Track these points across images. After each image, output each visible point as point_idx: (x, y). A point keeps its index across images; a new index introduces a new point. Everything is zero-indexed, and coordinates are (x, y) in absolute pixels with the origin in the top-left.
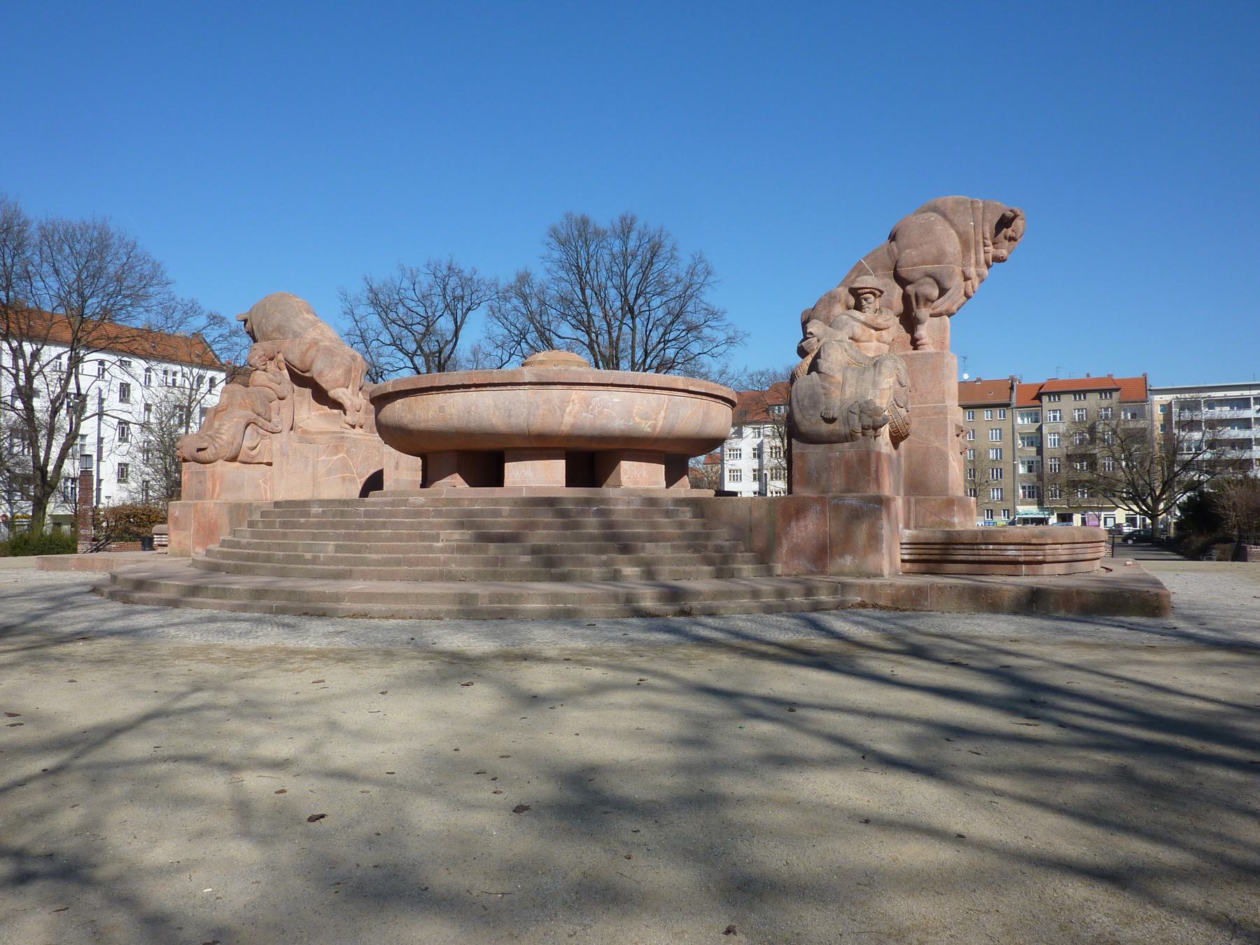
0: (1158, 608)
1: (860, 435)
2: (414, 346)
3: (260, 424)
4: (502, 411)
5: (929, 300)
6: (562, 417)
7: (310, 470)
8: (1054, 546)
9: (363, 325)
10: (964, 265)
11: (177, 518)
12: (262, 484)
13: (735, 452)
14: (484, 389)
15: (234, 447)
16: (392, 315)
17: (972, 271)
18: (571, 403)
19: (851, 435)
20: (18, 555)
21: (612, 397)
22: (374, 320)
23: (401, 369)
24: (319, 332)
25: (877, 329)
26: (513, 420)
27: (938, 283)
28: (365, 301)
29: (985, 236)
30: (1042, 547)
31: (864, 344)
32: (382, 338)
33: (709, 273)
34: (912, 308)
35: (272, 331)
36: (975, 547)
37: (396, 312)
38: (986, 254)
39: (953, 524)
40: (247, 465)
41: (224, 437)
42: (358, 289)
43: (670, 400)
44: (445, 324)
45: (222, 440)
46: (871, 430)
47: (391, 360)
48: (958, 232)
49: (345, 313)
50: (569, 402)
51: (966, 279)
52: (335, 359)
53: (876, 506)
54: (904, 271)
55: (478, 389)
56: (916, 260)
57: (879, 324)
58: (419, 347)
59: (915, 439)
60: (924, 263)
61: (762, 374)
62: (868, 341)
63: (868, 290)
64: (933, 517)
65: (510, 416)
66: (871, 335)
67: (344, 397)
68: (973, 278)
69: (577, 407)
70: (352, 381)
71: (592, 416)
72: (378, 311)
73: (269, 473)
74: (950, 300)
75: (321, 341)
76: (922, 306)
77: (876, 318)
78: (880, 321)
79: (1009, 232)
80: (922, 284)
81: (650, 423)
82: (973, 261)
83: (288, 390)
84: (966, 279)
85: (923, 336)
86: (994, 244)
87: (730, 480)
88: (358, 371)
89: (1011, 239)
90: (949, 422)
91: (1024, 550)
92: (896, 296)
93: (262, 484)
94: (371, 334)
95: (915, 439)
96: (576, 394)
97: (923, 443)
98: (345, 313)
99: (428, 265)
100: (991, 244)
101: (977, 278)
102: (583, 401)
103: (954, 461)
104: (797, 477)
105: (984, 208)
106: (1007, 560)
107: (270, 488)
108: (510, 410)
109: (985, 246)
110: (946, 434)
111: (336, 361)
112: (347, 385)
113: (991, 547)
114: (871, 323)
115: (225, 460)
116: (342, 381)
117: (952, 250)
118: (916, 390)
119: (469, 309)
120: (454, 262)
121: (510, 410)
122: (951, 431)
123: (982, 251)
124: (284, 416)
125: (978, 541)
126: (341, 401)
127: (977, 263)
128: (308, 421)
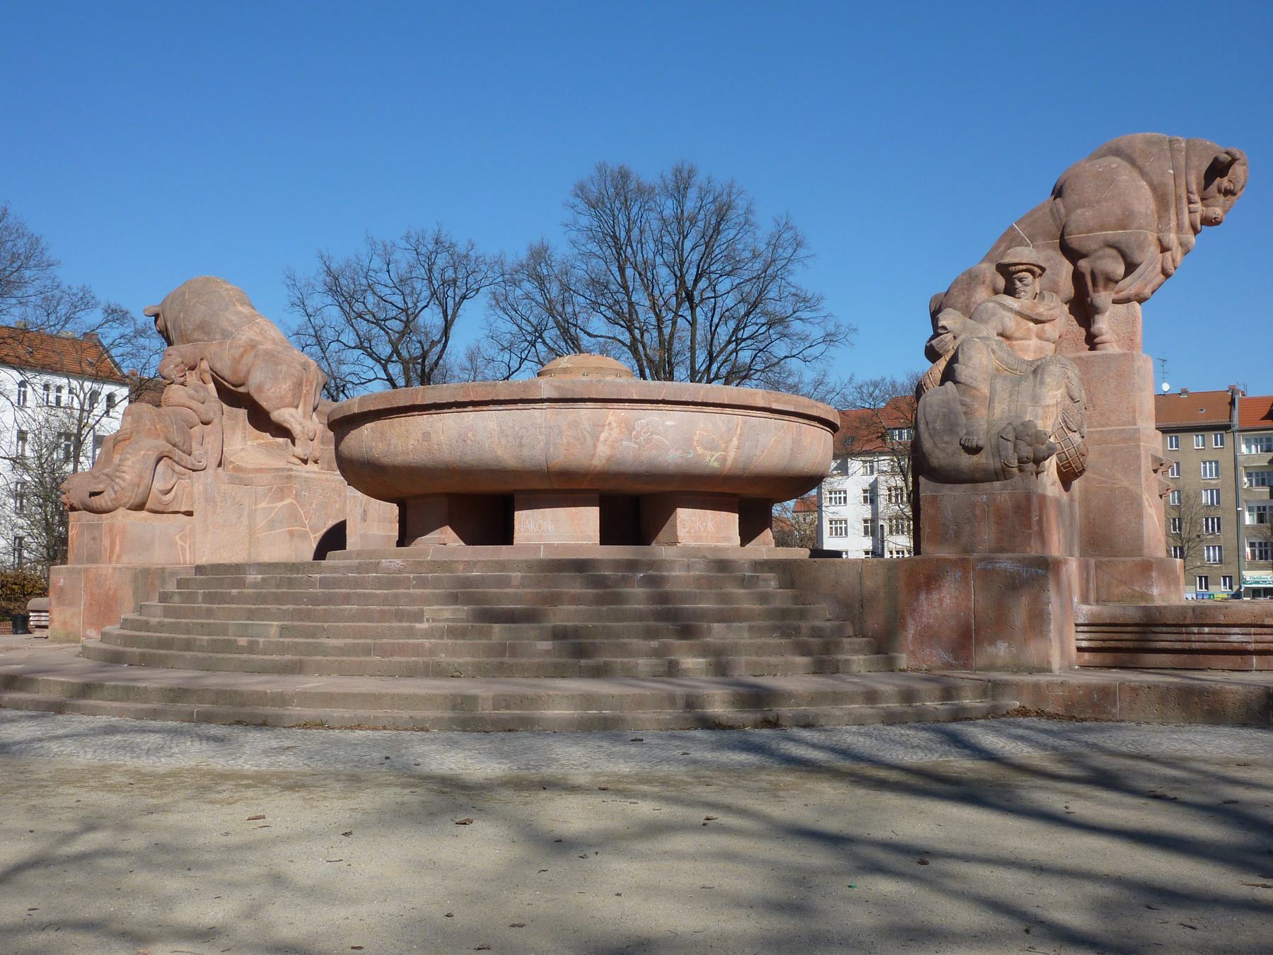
1: (1016, 470)
2: (389, 350)
3: (176, 459)
5: (1110, 280)
6: (595, 446)
9: (318, 321)
10: (1160, 231)
11: (62, 589)
12: (179, 542)
13: (838, 496)
14: (485, 408)
15: (140, 491)
16: (359, 307)
17: (1172, 238)
18: (606, 428)
21: (665, 418)
22: (333, 314)
23: (370, 381)
24: (258, 330)
25: (1037, 322)
27: (1124, 256)
28: (321, 288)
29: (1190, 190)
31: (1021, 342)
32: (344, 338)
35: (194, 330)
37: (364, 303)
38: (1192, 215)
41: (127, 477)
42: (311, 271)
44: (431, 318)
45: (124, 480)
46: (1031, 463)
47: (357, 369)
48: (1154, 188)
49: (293, 304)
50: (604, 426)
51: (1164, 249)
52: (279, 368)
53: (1040, 571)
54: (1074, 240)
55: (459, 410)
56: (1091, 224)
57: (1040, 314)
58: (396, 351)
60: (1102, 228)
61: (876, 385)
66: (1029, 329)
67: (292, 420)
68: (1174, 249)
70: (302, 400)
72: (338, 301)
73: (188, 527)
75: (261, 343)
76: (1101, 289)
77: (1035, 306)
79: (1224, 183)
80: (1100, 258)
81: (717, 455)
82: (1173, 224)
83: (214, 412)
84: (1164, 249)
85: (1104, 331)
86: (1203, 199)
87: (831, 534)
88: (311, 385)
90: (1142, 452)
91: (1255, 634)
92: (1064, 274)
93: (179, 542)
94: (329, 334)
96: (613, 415)
97: (1105, 482)
98: (293, 304)
99: (407, 238)
100: (1199, 200)
101: (1180, 248)
104: (928, 530)
108: (521, 438)
109: (1190, 202)
110: (1139, 469)
111: (281, 371)
112: (296, 404)
114: (1028, 312)
115: (129, 509)
116: (289, 399)
117: (1142, 209)
118: (1094, 407)
119: (464, 297)
120: (444, 232)
121: (521, 438)
122: (1146, 464)
123: (1186, 210)
124: (210, 446)
125: (1188, 621)
126: (288, 426)
127: (1180, 228)
128: (243, 454)
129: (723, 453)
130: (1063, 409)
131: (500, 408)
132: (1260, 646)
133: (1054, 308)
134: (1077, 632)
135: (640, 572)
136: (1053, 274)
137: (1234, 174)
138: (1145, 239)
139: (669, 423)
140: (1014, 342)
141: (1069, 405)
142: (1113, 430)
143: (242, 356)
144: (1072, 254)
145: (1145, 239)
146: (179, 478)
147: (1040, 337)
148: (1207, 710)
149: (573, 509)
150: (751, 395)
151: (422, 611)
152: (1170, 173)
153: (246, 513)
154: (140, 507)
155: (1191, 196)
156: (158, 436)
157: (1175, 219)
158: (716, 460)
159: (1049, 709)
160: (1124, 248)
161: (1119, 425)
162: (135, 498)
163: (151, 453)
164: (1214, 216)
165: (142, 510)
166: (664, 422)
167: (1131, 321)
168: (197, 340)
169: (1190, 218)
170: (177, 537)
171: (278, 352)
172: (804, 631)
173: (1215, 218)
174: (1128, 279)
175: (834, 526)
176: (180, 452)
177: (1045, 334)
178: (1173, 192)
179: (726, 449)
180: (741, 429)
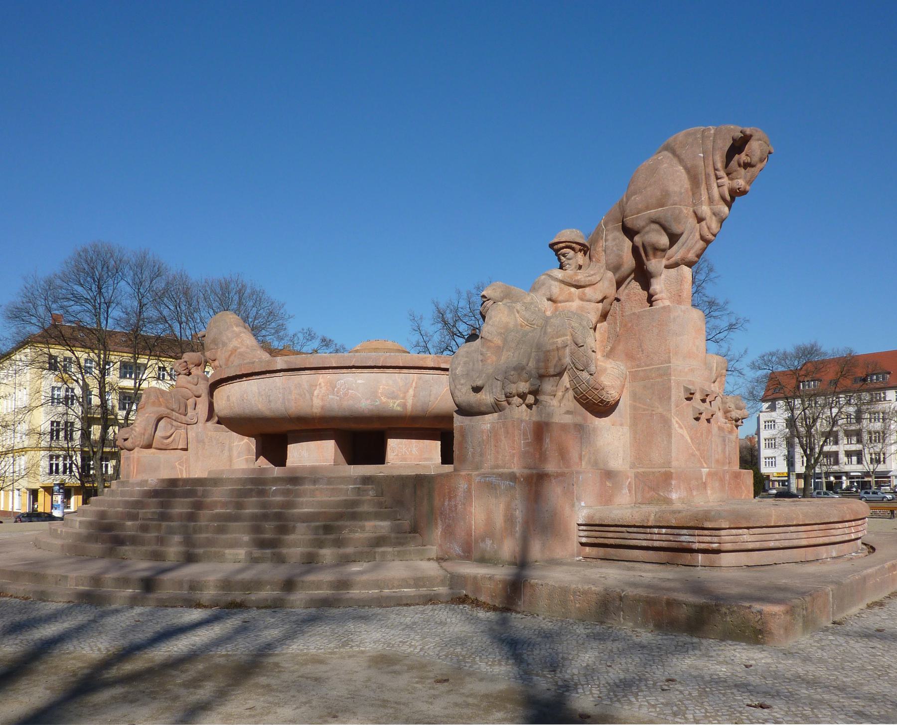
0: (761, 632)
1: (505, 403)
3: (174, 418)
4: (263, 397)
5: (658, 250)
6: (312, 399)
7: (226, 453)
8: (734, 531)
10: (694, 205)
13: (770, 424)
14: (251, 378)
15: (146, 437)
17: (705, 210)
18: (318, 387)
19: (496, 404)
20: (754, 487)
21: (357, 378)
25: (578, 287)
26: (273, 405)
27: (665, 229)
29: (716, 167)
30: (717, 533)
31: (563, 304)
33: (711, 270)
34: (643, 260)
35: (211, 343)
36: (648, 530)
38: (721, 188)
39: (668, 501)
40: (163, 451)
41: (137, 429)
43: (419, 379)
45: (135, 431)
46: (516, 397)
48: (688, 170)
50: (316, 386)
51: (700, 220)
53: (511, 483)
54: (630, 221)
55: (248, 379)
56: (640, 206)
57: (578, 281)
59: (640, 405)
60: (648, 208)
61: (772, 354)
62: (567, 301)
63: (563, 245)
64: (652, 493)
65: (270, 401)
66: (570, 293)
68: (708, 218)
69: (324, 389)
71: (338, 398)
73: (185, 457)
74: (685, 246)
75: (239, 348)
76: (651, 257)
77: (576, 274)
78: (581, 277)
79: (743, 157)
80: (647, 232)
81: (398, 402)
82: (704, 197)
84: (700, 220)
85: (657, 291)
86: (728, 174)
87: (766, 447)
89: (747, 165)
90: (673, 384)
91: (698, 535)
92: (626, 249)
95: (640, 405)
96: (323, 378)
97: (647, 410)
100: (725, 175)
101: (714, 218)
102: (329, 384)
103: (681, 428)
104: (457, 452)
105: (715, 134)
106: (680, 547)
107: (186, 469)
109: (717, 178)
110: (670, 398)
113: (664, 531)
114: (568, 280)
117: (677, 189)
118: (642, 351)
122: (677, 394)
123: (715, 185)
125: (650, 524)
127: (711, 200)
129: (402, 401)
130: (571, 353)
131: (258, 377)
132: (703, 546)
133: (592, 275)
134: (579, 530)
135: (274, 486)
136: (618, 250)
137: (750, 149)
138: (679, 213)
139: (359, 382)
140: (559, 304)
141: (574, 349)
142: (653, 368)
143: (230, 356)
144: (629, 232)
145: (679, 213)
146: (176, 429)
147: (582, 299)
148: (579, 608)
149: (319, 442)
150: (423, 359)
151: (138, 513)
152: (700, 156)
153: (227, 448)
154: (149, 446)
155: (717, 172)
156: (160, 405)
157: (706, 193)
158: (398, 405)
159: (482, 598)
160: (664, 222)
161: (658, 364)
162: (144, 440)
163: (152, 415)
164: (738, 187)
165: (151, 448)
166: (356, 381)
167: (680, 281)
168: (212, 349)
169: (719, 191)
170: (177, 464)
171: (246, 353)
172: (367, 529)
173: (739, 189)
174: (675, 247)
175: (770, 442)
176: (177, 414)
177: (585, 296)
178: (703, 172)
179: (404, 398)
180: (416, 383)
